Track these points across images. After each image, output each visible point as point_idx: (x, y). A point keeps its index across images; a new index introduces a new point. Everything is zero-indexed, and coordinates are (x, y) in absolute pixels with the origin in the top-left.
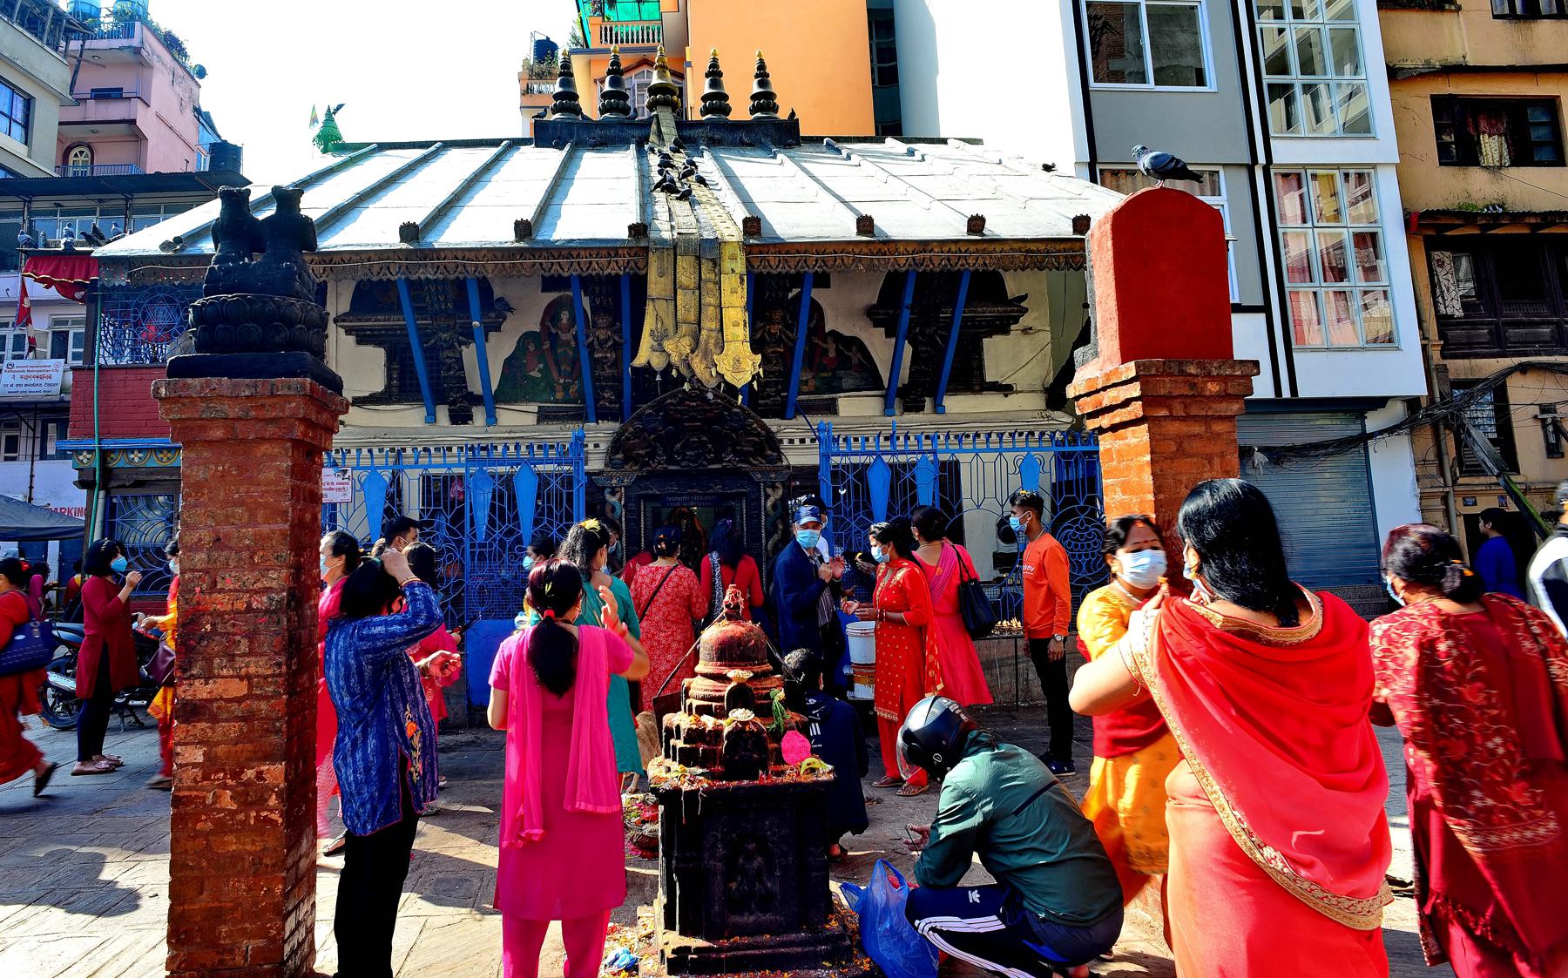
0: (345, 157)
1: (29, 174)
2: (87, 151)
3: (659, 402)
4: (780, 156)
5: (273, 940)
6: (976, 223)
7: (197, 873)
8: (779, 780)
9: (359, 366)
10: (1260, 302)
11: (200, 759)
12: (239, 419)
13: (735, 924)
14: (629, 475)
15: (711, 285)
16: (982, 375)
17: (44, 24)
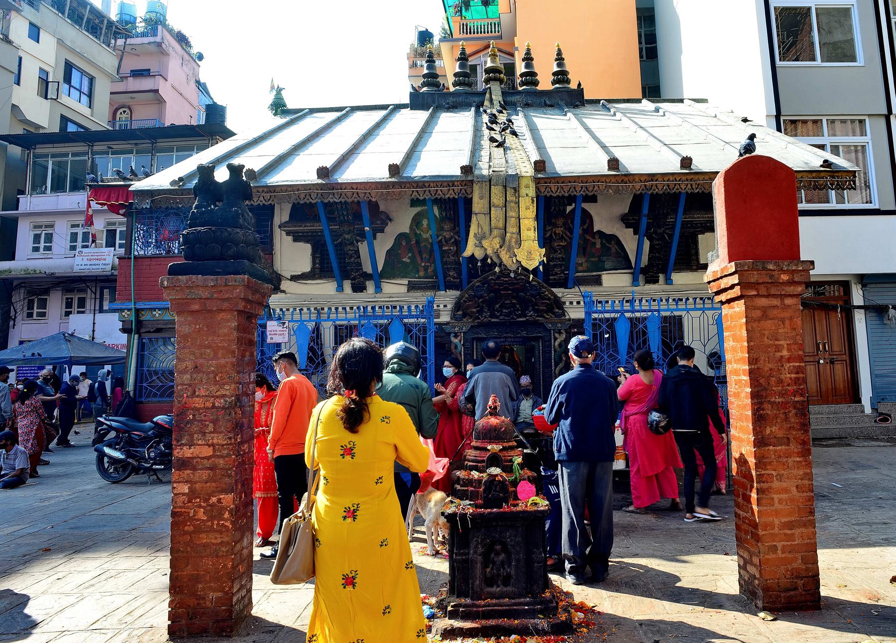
0: (287, 119)
1: (94, 128)
2: (128, 111)
3: (484, 278)
4: (569, 114)
5: (226, 593)
6: (686, 162)
7: (185, 554)
8: (513, 509)
9: (292, 256)
11: (187, 491)
12: (207, 299)
13: (488, 593)
14: (466, 325)
15: (513, 204)
16: (698, 260)
17: (101, 29)
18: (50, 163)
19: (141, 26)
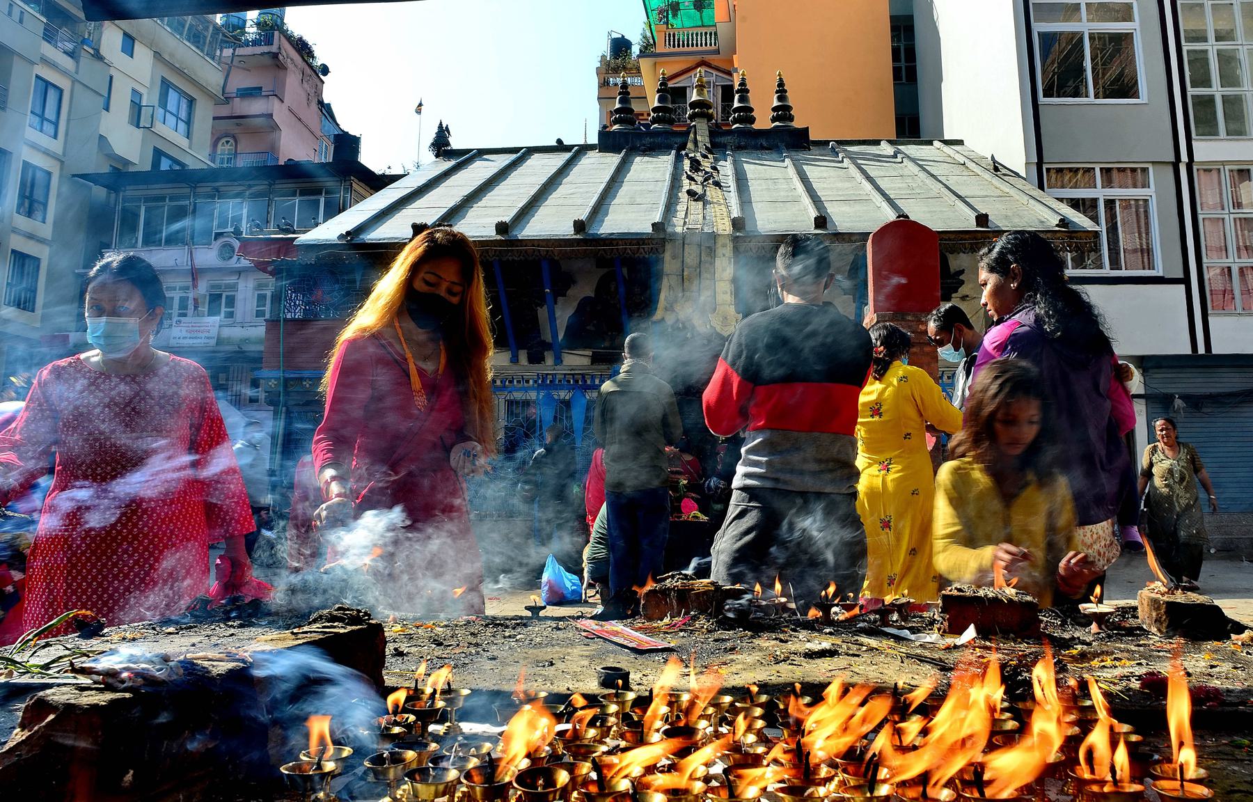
1: (192, 164)
2: (232, 141)
10: (1181, 276)
17: (205, 37)
18: (143, 209)
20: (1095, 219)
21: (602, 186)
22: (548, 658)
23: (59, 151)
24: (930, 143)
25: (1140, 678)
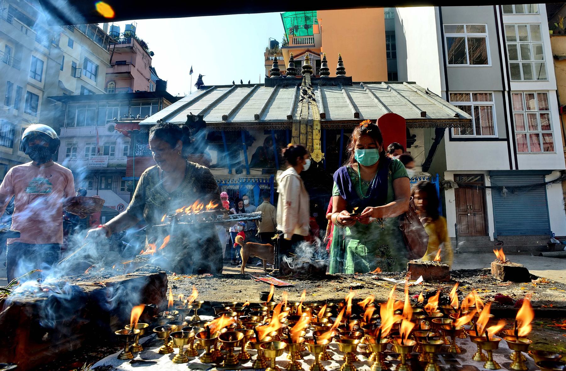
0: (205, 91)
2: (114, 83)
4: (343, 91)
6: (423, 114)
10: (506, 137)
19: (122, 37)
20: (470, 114)
21: (266, 101)
22: (239, 289)
23: (42, 87)
24: (402, 83)
25: (493, 297)
